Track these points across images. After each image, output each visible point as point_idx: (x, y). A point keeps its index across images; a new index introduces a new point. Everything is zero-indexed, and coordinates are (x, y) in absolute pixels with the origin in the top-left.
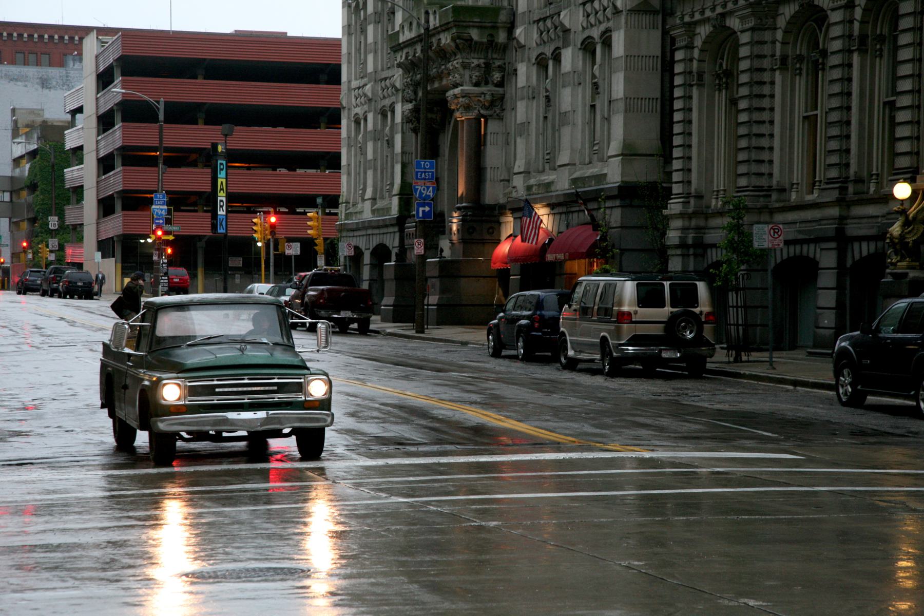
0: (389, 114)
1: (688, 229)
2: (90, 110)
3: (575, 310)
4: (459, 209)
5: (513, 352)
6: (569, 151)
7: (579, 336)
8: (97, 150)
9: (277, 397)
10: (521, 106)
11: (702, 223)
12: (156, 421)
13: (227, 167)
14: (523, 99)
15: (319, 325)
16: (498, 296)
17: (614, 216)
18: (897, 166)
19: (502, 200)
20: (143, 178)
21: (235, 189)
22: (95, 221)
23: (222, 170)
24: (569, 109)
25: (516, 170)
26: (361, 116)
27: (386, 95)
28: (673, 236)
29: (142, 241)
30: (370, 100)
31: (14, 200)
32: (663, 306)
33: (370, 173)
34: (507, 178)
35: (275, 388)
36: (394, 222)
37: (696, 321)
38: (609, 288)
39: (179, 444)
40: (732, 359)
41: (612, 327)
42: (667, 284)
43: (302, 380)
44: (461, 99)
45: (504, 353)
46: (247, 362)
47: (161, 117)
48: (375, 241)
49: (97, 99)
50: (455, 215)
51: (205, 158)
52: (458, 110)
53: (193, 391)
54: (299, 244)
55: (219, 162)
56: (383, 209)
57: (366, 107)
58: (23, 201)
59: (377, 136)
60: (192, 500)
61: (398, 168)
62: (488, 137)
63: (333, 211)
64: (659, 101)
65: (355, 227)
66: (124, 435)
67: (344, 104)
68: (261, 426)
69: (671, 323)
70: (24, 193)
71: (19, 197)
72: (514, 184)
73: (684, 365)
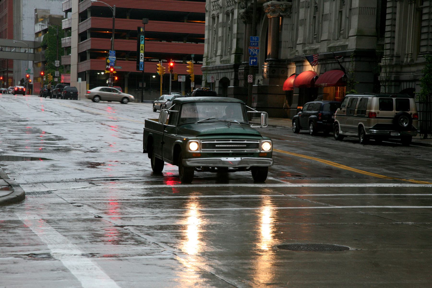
0: (231, 15)
1: (392, 72)
2: (75, 10)
3: (344, 111)
4: (268, 61)
5: (308, 131)
6: (327, 33)
7: (343, 123)
8: (78, 30)
9: (246, 150)
10: (302, 12)
11: (399, 70)
12: (186, 161)
13: (145, 40)
14: (303, 7)
15: (262, 114)
16: (286, 104)
17: (350, 66)
18: (421, 51)
19: (289, 57)
20: (102, 44)
21: (147, 51)
22: (76, 63)
23: (142, 40)
24: (328, 12)
25: (298, 42)
26: (216, 15)
27: (229, 5)
28: (383, 75)
29: (98, 74)
30: (221, 8)
31: (35, 52)
32: (392, 110)
33: (220, 43)
34: (292, 46)
35: (245, 146)
36: (232, 67)
37: (409, 118)
38: (364, 101)
39: (196, 173)
40: (422, 137)
41: (365, 120)
42: (394, 99)
43: (259, 142)
44: (271, 7)
45: (301, 131)
46: (231, 132)
47: (114, 14)
48: (221, 76)
49: (79, 5)
50: (266, 64)
51: (134, 35)
52: (269, 13)
53: (204, 146)
54: (185, 76)
55: (141, 36)
56: (226, 61)
57: (218, 11)
58: (40, 53)
59: (224, 25)
60: (202, 202)
61: (235, 41)
62: (283, 26)
63: (200, 62)
64: (376, 9)
65: (211, 69)
66: (157, 167)
67: (207, 9)
68: (238, 165)
69: (396, 119)
70: (41, 50)
71: (38, 51)
72: (297, 49)
73: (400, 140)
